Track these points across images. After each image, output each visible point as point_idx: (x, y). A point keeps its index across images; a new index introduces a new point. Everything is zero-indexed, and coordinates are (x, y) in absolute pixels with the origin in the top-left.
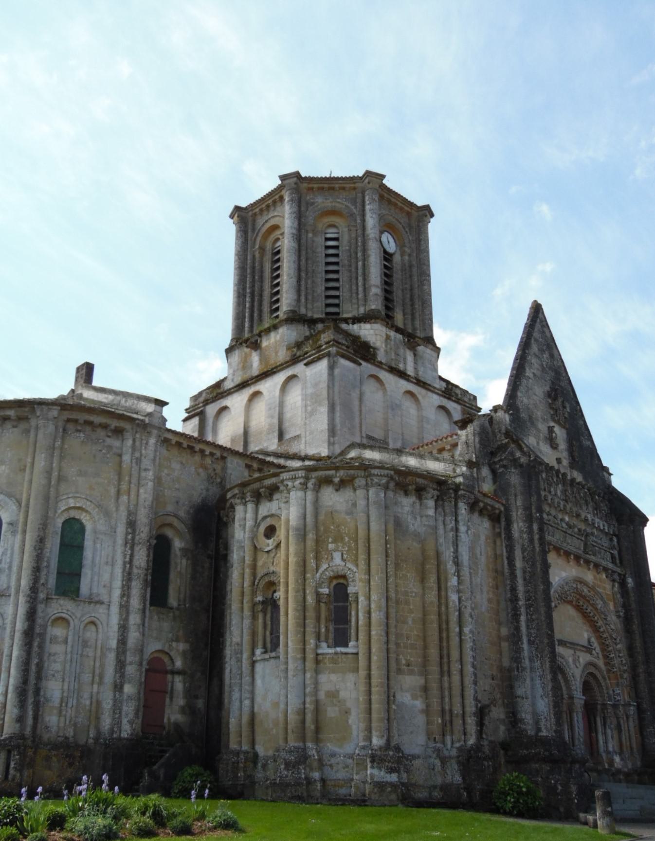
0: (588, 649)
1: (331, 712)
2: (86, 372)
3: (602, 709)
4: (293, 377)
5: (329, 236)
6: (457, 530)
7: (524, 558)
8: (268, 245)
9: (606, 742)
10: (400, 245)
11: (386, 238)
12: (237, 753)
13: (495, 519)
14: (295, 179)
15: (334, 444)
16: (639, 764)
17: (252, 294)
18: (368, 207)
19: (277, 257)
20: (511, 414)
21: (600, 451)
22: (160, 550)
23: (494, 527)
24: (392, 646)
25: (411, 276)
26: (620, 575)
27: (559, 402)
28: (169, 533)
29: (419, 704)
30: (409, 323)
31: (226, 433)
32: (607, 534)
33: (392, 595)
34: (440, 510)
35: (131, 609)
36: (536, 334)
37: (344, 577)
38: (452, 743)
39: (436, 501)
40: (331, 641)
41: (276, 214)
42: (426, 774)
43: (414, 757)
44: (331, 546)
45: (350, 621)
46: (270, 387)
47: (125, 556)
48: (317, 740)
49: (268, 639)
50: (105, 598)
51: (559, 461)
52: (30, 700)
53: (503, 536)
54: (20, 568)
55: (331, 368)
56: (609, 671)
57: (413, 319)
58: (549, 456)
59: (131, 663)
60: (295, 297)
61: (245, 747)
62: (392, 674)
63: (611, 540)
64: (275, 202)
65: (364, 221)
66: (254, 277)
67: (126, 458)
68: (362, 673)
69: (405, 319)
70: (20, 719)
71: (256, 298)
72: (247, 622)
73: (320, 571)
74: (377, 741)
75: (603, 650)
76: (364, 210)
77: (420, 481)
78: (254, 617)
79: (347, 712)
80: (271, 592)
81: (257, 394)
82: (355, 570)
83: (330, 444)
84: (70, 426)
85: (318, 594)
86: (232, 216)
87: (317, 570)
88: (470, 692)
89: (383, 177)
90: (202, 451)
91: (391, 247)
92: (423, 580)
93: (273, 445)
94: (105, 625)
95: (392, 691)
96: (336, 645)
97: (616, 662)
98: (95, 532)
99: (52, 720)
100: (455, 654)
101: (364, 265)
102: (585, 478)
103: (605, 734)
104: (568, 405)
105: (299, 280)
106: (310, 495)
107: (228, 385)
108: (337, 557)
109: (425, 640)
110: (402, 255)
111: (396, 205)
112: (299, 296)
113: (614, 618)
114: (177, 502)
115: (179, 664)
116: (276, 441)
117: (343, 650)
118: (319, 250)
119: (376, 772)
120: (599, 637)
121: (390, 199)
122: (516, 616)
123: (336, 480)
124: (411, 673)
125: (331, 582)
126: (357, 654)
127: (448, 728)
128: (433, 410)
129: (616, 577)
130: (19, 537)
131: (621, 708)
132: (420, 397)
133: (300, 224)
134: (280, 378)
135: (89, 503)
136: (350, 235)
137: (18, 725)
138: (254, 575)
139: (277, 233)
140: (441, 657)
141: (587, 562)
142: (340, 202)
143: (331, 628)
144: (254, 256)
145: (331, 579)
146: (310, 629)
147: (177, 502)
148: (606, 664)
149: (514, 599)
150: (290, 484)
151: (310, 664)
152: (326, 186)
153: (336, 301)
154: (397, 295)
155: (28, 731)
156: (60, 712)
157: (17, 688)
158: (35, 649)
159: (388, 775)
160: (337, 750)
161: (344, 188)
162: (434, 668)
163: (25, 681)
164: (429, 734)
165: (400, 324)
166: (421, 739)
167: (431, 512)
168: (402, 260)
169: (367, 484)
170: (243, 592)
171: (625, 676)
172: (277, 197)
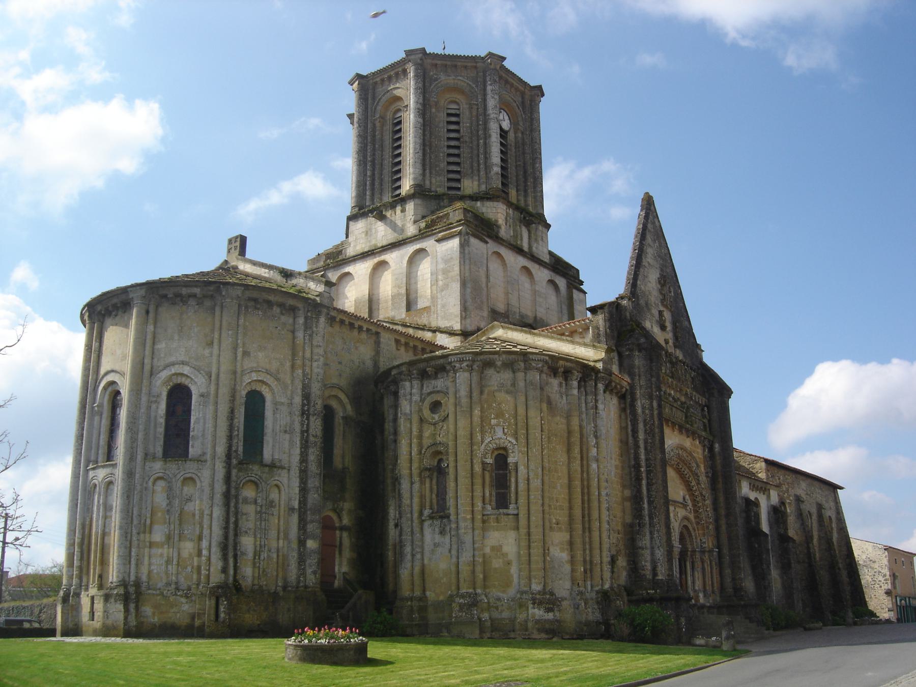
0: (685, 506)
1: (496, 564)
2: (240, 244)
3: (692, 556)
4: (422, 251)
5: (449, 111)
6: (596, 408)
7: (646, 430)
8: (389, 115)
9: (694, 582)
10: (514, 123)
11: (503, 116)
12: (411, 599)
13: (622, 397)
14: (421, 55)
15: (465, 318)
16: (718, 599)
17: (373, 162)
18: (489, 88)
19: (398, 128)
20: (633, 302)
21: (695, 331)
22: (328, 415)
23: (620, 403)
24: (546, 508)
25: (524, 153)
26: (709, 441)
27: (666, 289)
28: (334, 404)
29: (565, 556)
30: (522, 198)
31: (352, 297)
32: (700, 405)
33: (546, 465)
34: (582, 389)
35: (309, 473)
36: (650, 226)
37: (505, 449)
38: (592, 586)
39: (579, 382)
40: (494, 503)
41: (398, 85)
42: (567, 615)
43: (563, 599)
44: (493, 422)
45: (510, 487)
46: (397, 259)
47: (302, 425)
48: (485, 587)
49: (435, 501)
50: (285, 463)
51: (667, 342)
52: (231, 554)
53: (628, 411)
54: (214, 436)
55: (462, 246)
56: (698, 523)
57: (526, 196)
58: (660, 336)
59: (312, 521)
60: (421, 172)
61: (418, 593)
62: (547, 531)
63: (703, 410)
64: (397, 74)
65: (485, 100)
66: (374, 146)
67: (300, 334)
68: (523, 531)
69: (518, 196)
70: (224, 570)
71: (377, 167)
72: (416, 486)
73: (484, 444)
74: (536, 587)
75: (694, 506)
76: (485, 90)
77: (569, 364)
78: (422, 482)
79: (509, 563)
80: (436, 461)
81: (383, 264)
82: (515, 442)
83: (463, 318)
84: (251, 304)
85: (483, 463)
86: (351, 83)
87: (482, 442)
88: (606, 546)
89: (504, 59)
90: (360, 328)
91: (506, 125)
92: (569, 451)
93: (401, 314)
94: (286, 486)
95: (547, 546)
96: (498, 508)
97: (703, 516)
98: (275, 403)
99: (247, 571)
100: (595, 514)
101: (485, 144)
102: (684, 356)
103: (693, 576)
104: (672, 290)
105: (424, 155)
106: (475, 378)
107: (350, 251)
108: (499, 433)
109: (570, 502)
110: (515, 133)
111: (512, 85)
112: (424, 170)
113: (704, 478)
114: (340, 375)
115: (346, 521)
116: (404, 310)
117: (505, 511)
118: (441, 125)
119: (536, 610)
120: (692, 495)
121: (508, 79)
122: (638, 479)
123: (499, 363)
124: (560, 530)
125: (493, 452)
126: (517, 515)
127: (589, 575)
128: (545, 283)
129: (706, 443)
130: (211, 408)
131: (707, 555)
132: (532, 270)
133: (424, 99)
134: (410, 249)
135: (269, 377)
136: (471, 113)
137: (223, 575)
138: (420, 445)
139: (399, 104)
140: (583, 517)
141: (687, 430)
142: (462, 80)
143: (494, 493)
144: (374, 125)
145: (497, 449)
146: (478, 493)
147: (340, 375)
148: (696, 517)
149: (637, 466)
150: (457, 365)
151: (478, 524)
152: (449, 63)
153: (456, 151)
154: (512, 170)
155: (231, 579)
156: (254, 564)
157: (220, 544)
158: (232, 509)
159: (546, 614)
160: (501, 595)
161: (466, 67)
162: (578, 526)
163: (226, 537)
164: (573, 580)
165: (514, 200)
166: (568, 585)
167: (575, 392)
168: (516, 138)
169: (526, 369)
170: (411, 460)
171: (711, 527)
172: (400, 69)
